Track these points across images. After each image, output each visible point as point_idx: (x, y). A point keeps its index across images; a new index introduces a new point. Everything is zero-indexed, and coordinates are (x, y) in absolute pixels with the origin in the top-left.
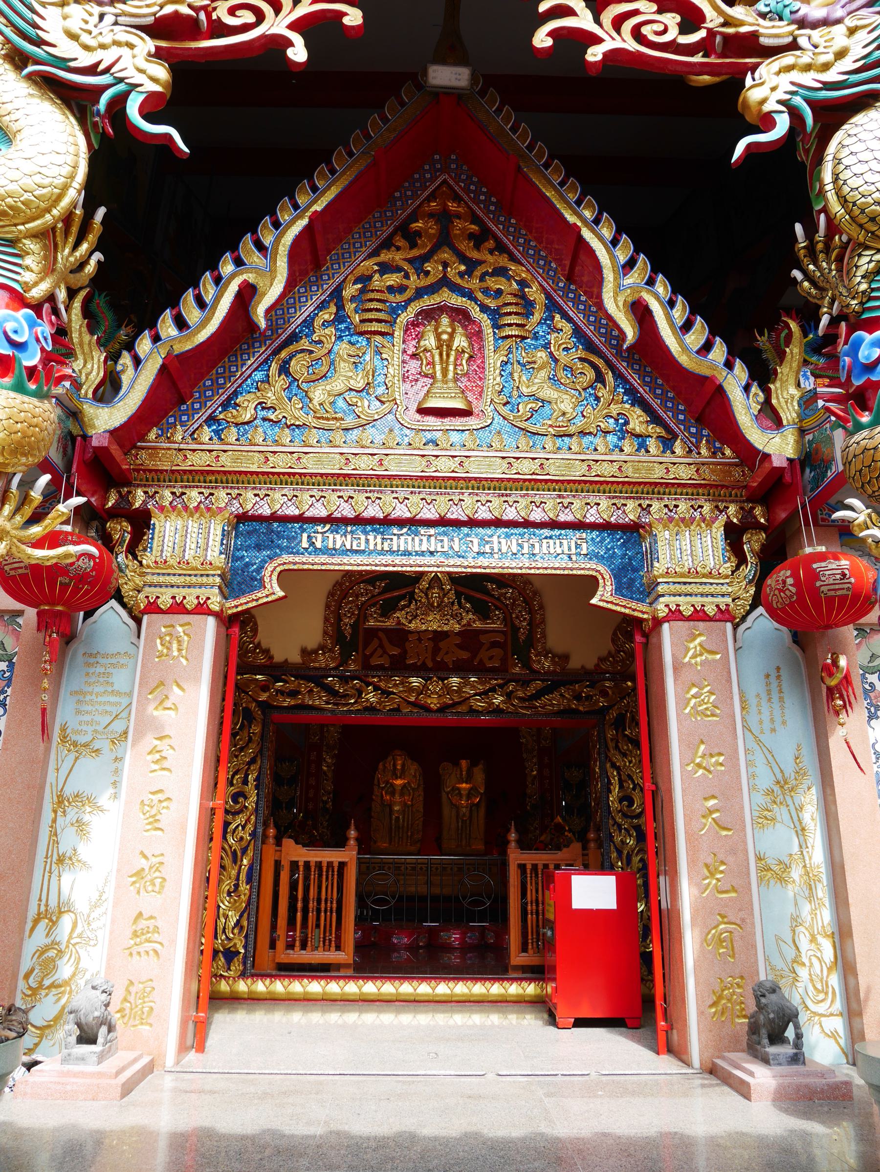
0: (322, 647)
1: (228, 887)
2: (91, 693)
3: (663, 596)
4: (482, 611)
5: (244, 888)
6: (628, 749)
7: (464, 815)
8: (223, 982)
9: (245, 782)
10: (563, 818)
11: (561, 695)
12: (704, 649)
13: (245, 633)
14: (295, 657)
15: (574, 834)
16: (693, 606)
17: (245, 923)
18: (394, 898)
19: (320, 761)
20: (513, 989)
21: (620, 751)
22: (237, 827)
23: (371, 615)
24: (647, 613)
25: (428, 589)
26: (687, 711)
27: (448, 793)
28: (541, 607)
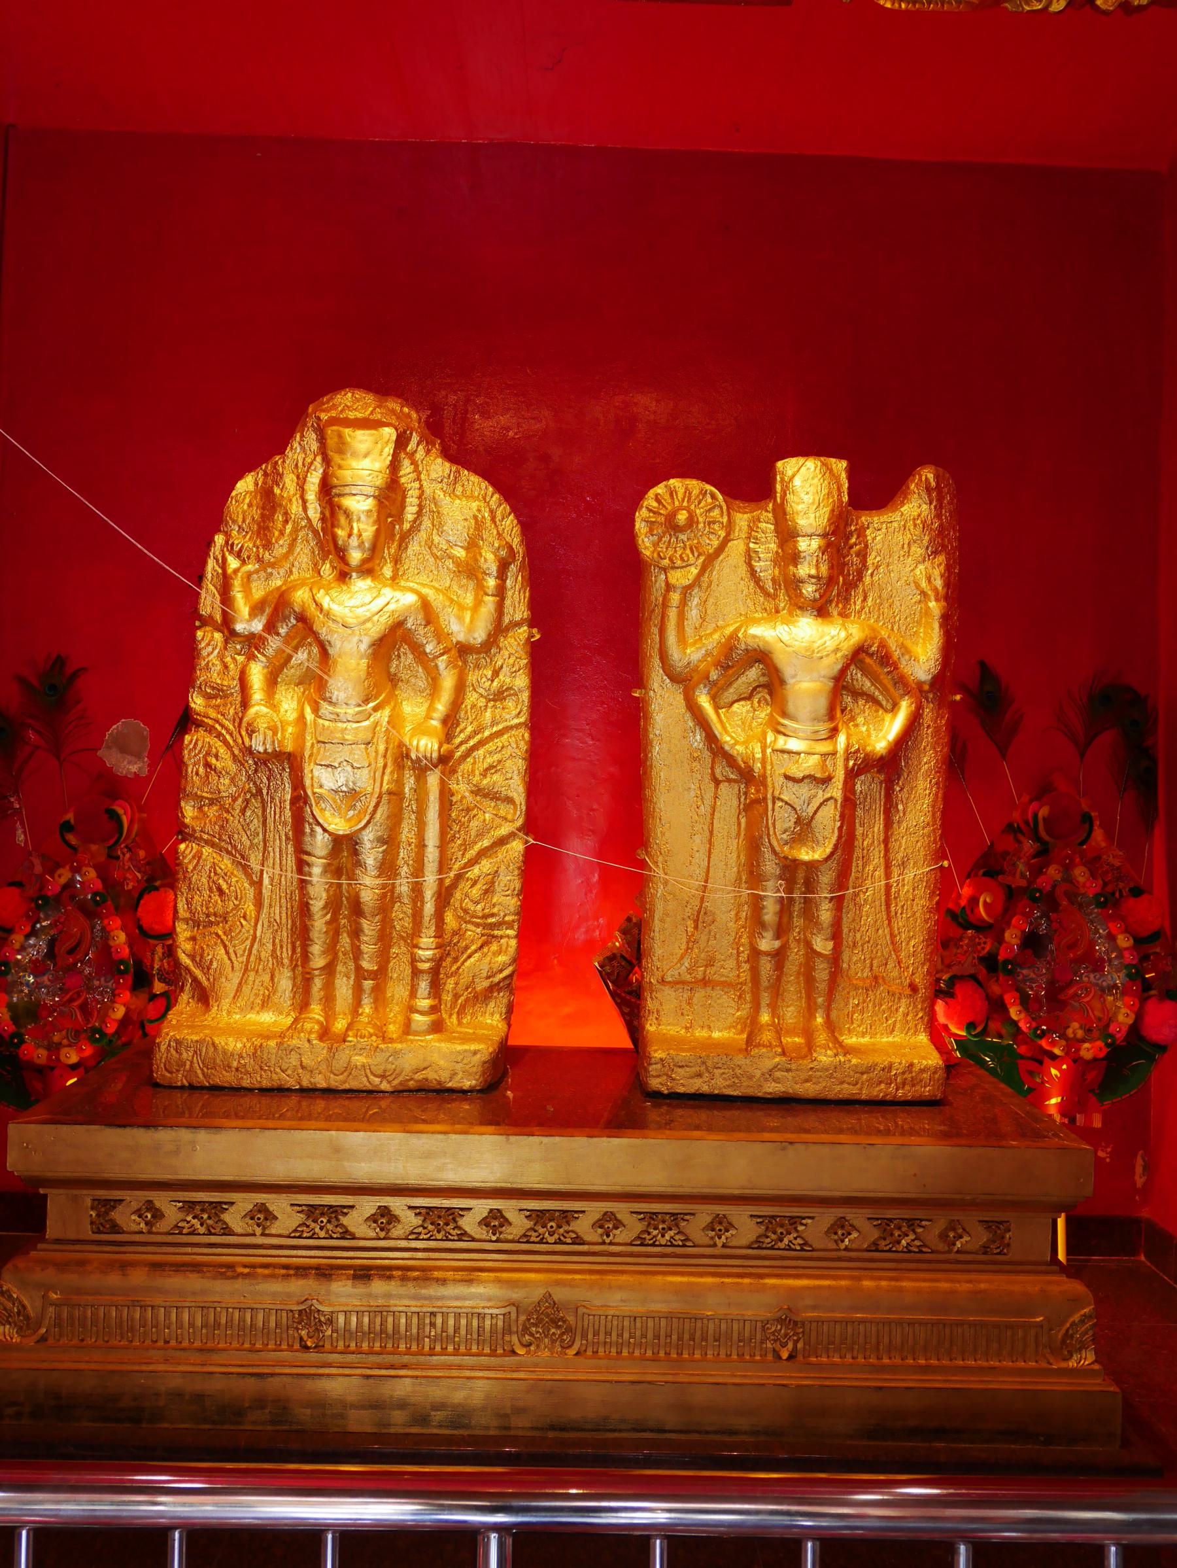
2: (215, 1059)
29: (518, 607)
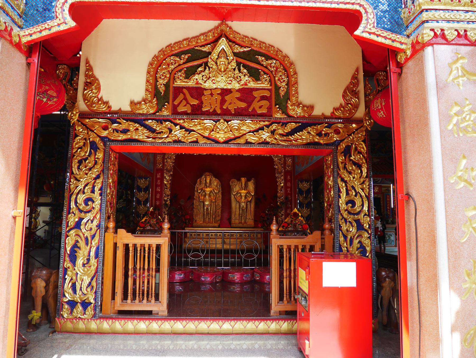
0: (144, 100)
1: (82, 261)
3: (427, 21)
4: (255, 75)
5: (93, 261)
6: (353, 169)
7: (243, 206)
8: (81, 322)
9: (93, 192)
10: (299, 210)
11: (308, 132)
12: (466, 71)
13: (92, 90)
14: (126, 108)
15: (304, 218)
16: (456, 30)
17: (94, 283)
18: (203, 254)
19: (162, 178)
20: (273, 326)
21: (347, 171)
22: (88, 221)
23: (178, 78)
24: (406, 44)
25: (217, 59)
26: (450, 127)
27: (234, 195)
28: (295, 73)
29: (220, 190)
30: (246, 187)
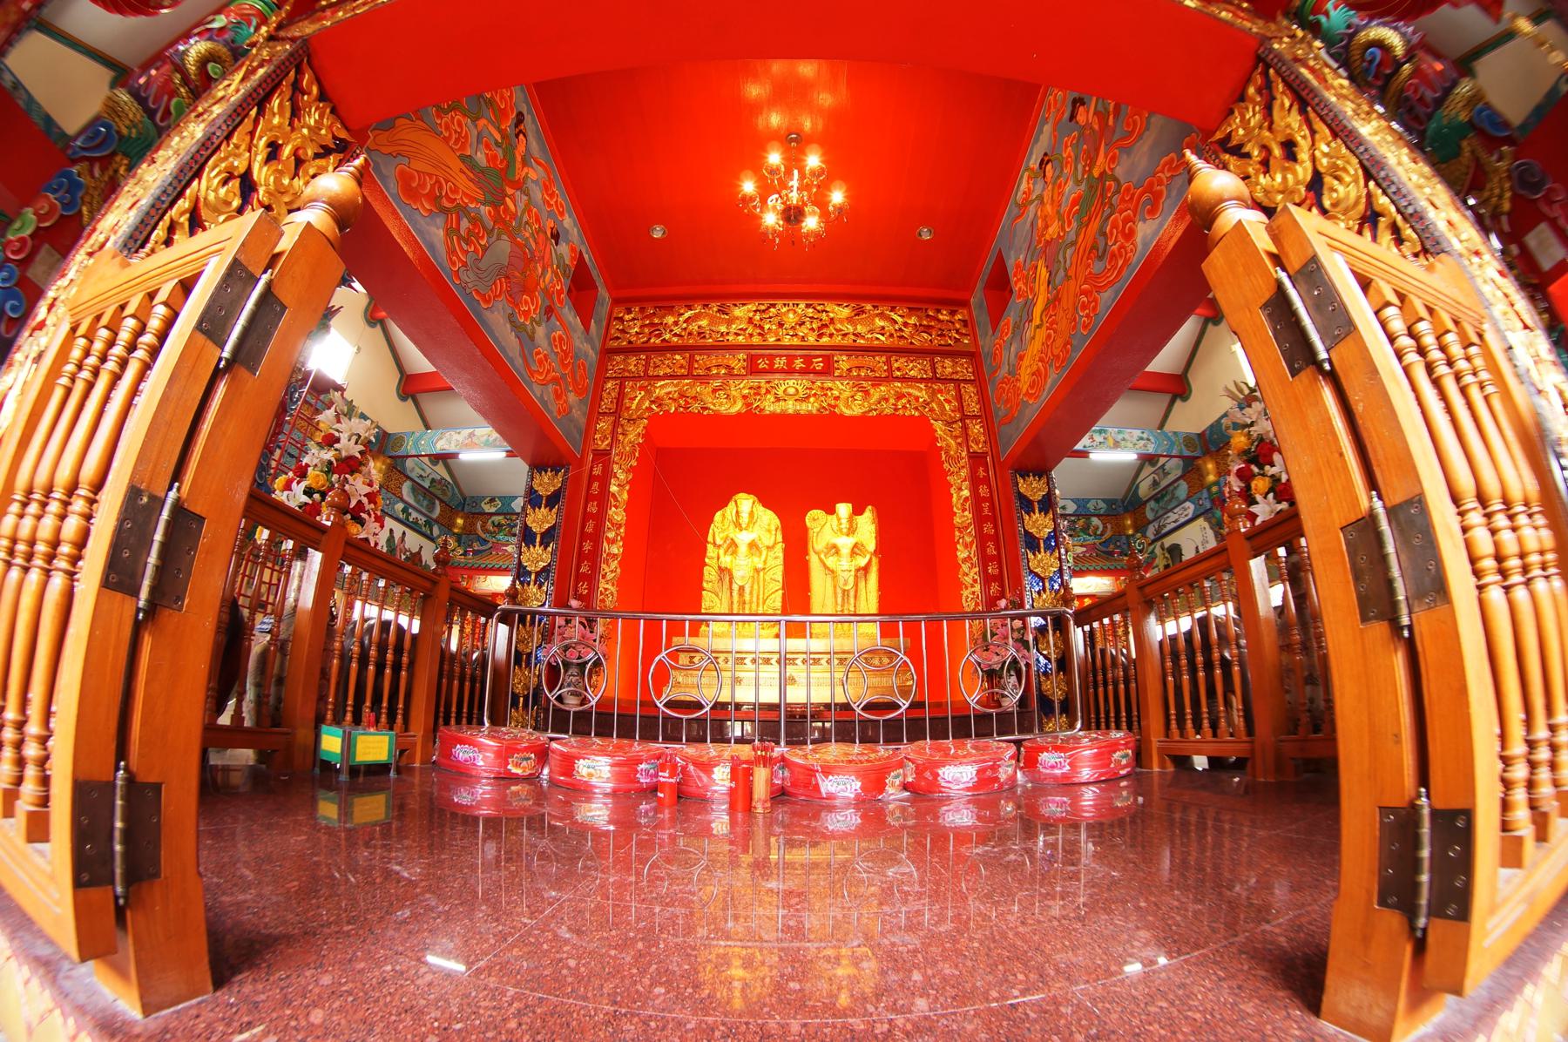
29: (780, 538)
30: (852, 530)
